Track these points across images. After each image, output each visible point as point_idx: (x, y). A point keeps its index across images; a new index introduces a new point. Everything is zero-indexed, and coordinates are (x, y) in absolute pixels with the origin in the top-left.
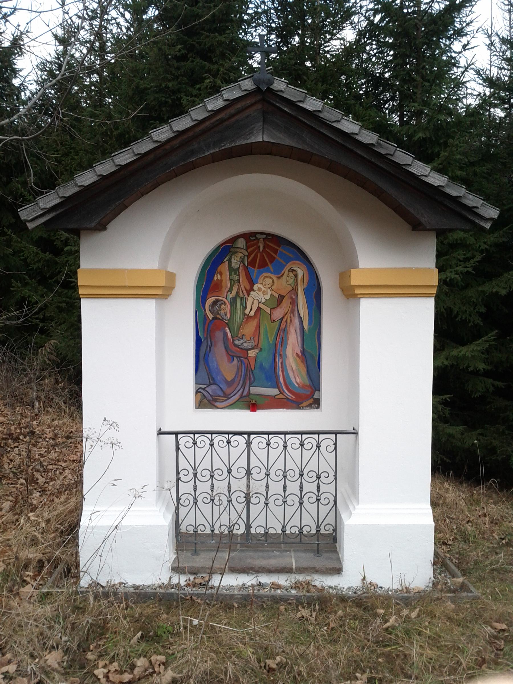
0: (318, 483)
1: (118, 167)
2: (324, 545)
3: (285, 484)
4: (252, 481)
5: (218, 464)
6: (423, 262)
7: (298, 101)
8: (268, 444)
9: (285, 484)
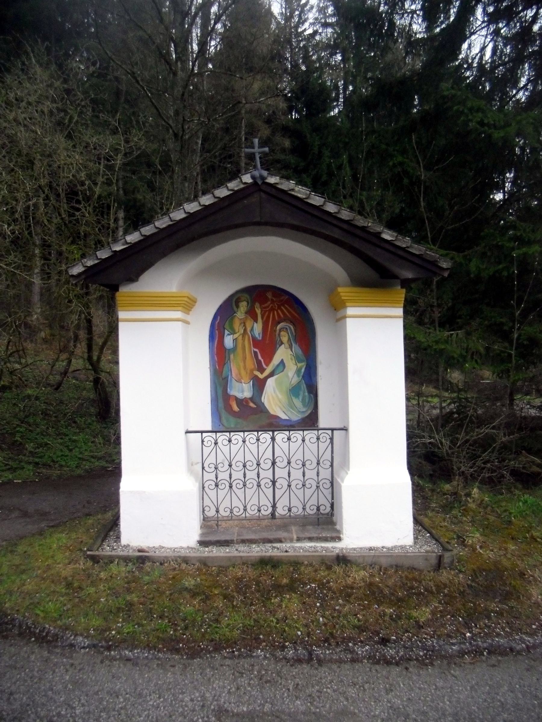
2: (326, 521)
3: (258, 472)
5: (249, 457)
7: (290, 190)
8: (258, 440)
9: (258, 472)
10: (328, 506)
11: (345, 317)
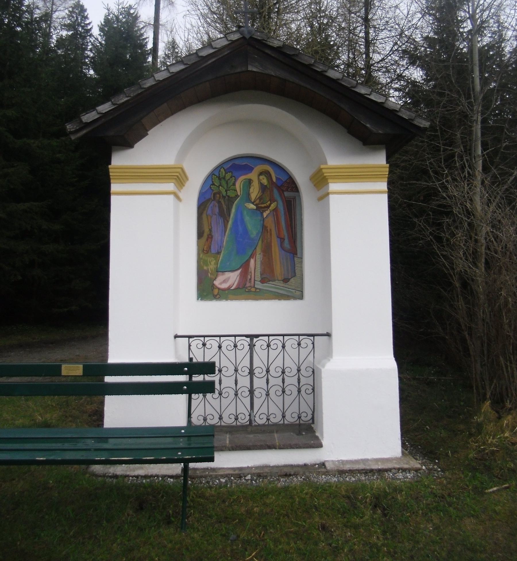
0: (299, 376)
1: (230, 42)
2: (305, 431)
4: (255, 378)
5: (289, 363)
6: (379, 160)
10: (310, 413)
11: (328, 194)
